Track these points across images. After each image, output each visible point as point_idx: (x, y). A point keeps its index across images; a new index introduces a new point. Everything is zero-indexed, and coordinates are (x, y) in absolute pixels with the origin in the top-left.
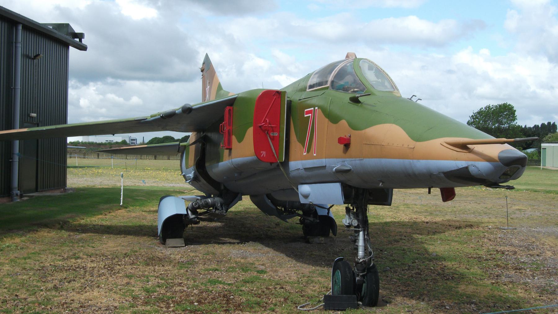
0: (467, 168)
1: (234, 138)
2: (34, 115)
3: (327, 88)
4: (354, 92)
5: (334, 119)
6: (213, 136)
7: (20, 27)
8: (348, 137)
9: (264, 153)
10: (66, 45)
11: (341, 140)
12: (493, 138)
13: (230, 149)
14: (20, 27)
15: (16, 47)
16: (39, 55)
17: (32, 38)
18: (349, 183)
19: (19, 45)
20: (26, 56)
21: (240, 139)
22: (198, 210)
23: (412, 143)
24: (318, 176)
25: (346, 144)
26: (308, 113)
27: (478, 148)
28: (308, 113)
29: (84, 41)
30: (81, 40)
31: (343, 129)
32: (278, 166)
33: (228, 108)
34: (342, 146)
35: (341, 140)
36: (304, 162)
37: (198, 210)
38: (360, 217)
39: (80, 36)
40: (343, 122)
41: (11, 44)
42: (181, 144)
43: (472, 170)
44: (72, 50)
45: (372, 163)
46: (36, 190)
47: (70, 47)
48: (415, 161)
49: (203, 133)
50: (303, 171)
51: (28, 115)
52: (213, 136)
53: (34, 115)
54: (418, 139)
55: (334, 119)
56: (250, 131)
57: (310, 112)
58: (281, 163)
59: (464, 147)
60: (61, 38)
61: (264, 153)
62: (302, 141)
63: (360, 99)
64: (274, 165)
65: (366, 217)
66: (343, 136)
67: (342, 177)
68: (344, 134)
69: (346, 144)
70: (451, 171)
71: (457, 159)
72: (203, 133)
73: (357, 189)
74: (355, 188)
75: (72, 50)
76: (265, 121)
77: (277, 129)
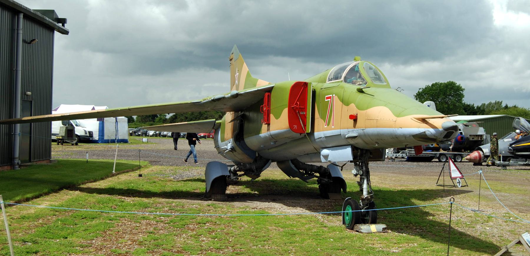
0: (425, 132)
1: (272, 116)
2: (29, 93)
3: (342, 81)
4: (360, 84)
5: (345, 102)
6: (251, 115)
7: (21, 16)
8: (355, 114)
9: (295, 126)
10: (51, 29)
11: (351, 117)
12: (443, 115)
13: (269, 124)
14: (21, 16)
15: (18, 33)
16: (34, 40)
17: (29, 24)
18: (357, 146)
19: (21, 32)
20: (24, 41)
21: (277, 117)
22: (238, 173)
23: (395, 118)
24: (336, 142)
25: (354, 118)
26: (327, 98)
27: (431, 121)
28: (327, 98)
29: (67, 27)
30: (63, 25)
31: (353, 109)
32: (305, 136)
33: (267, 94)
34: (352, 121)
35: (351, 117)
36: (325, 132)
37: (238, 173)
38: (364, 169)
39: (63, 21)
40: (353, 105)
41: (13, 31)
42: (217, 122)
43: (427, 133)
44: (57, 34)
45: (371, 130)
46: (30, 161)
47: (55, 31)
48: (396, 129)
49: (241, 112)
50: (324, 139)
51: (25, 94)
52: (251, 115)
53: (29, 93)
54: (398, 115)
55: (345, 102)
56: (286, 111)
57: (330, 98)
58: (308, 134)
59: (424, 120)
60: (48, 24)
61: (295, 126)
62: (323, 117)
63: (363, 90)
64: (303, 135)
65: (368, 169)
66: (352, 114)
67: (352, 142)
68: (354, 113)
69: (354, 118)
70: (417, 135)
71: (419, 127)
72: (241, 112)
73: (362, 150)
74: (360, 149)
75: (57, 34)
76: (296, 104)
77: (305, 109)
